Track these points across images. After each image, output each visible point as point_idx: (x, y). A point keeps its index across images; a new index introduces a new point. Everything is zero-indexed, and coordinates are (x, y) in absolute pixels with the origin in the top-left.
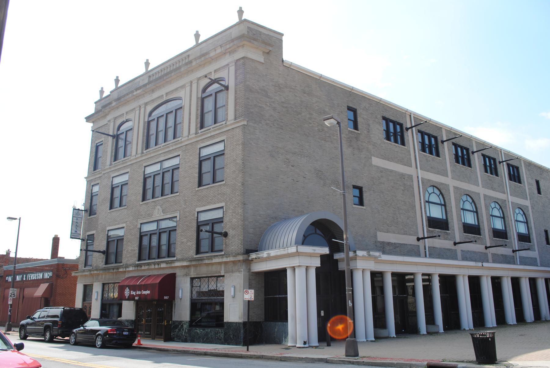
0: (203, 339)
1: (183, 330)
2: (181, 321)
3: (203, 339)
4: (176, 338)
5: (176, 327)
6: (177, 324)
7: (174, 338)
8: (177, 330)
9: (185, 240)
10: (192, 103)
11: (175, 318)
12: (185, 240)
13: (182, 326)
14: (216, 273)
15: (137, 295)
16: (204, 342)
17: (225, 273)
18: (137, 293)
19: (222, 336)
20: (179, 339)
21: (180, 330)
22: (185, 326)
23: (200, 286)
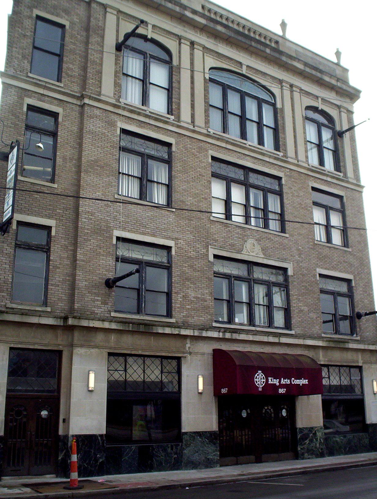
0: (345, 448)
1: (317, 440)
2: (312, 428)
3: (345, 448)
4: (306, 455)
5: (305, 437)
6: (306, 431)
7: (303, 454)
8: (307, 442)
9: (306, 309)
10: (196, 92)
11: (301, 423)
12: (306, 309)
13: (315, 434)
14: (354, 362)
15: (282, 386)
16: (346, 453)
17: (363, 363)
18: (283, 382)
19: (367, 441)
20: (312, 454)
21: (311, 441)
22: (319, 434)
23: (329, 378)
